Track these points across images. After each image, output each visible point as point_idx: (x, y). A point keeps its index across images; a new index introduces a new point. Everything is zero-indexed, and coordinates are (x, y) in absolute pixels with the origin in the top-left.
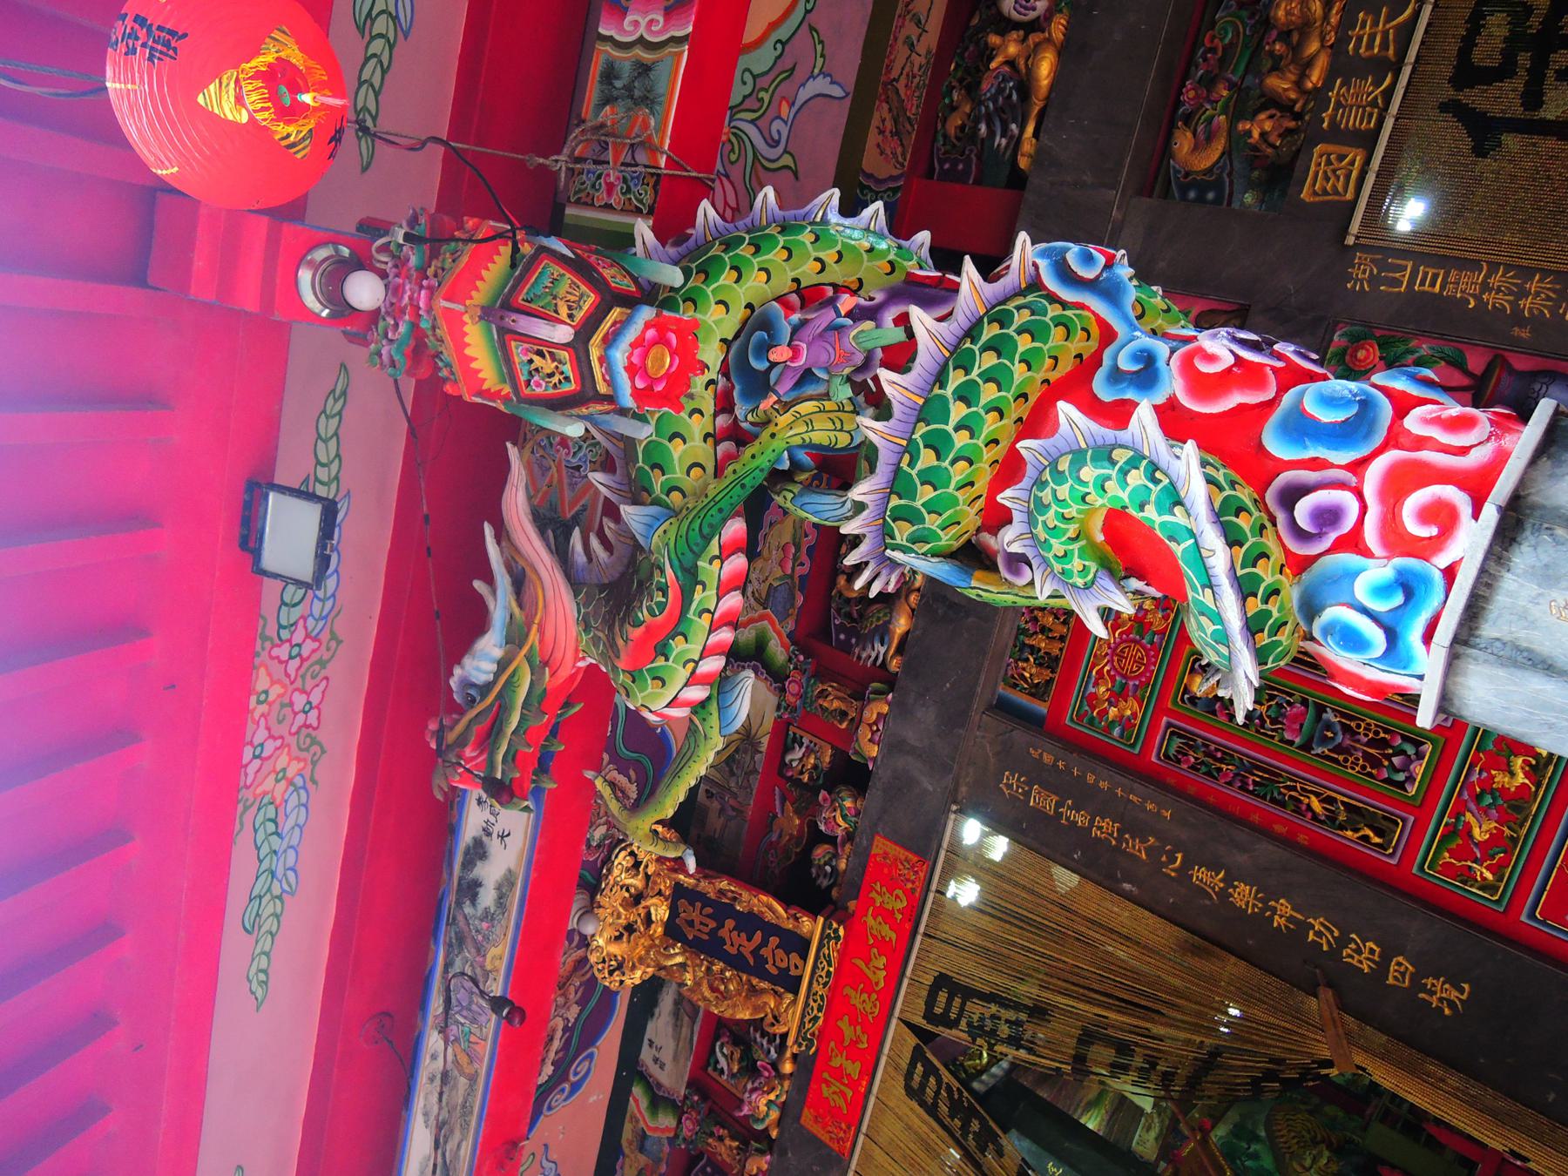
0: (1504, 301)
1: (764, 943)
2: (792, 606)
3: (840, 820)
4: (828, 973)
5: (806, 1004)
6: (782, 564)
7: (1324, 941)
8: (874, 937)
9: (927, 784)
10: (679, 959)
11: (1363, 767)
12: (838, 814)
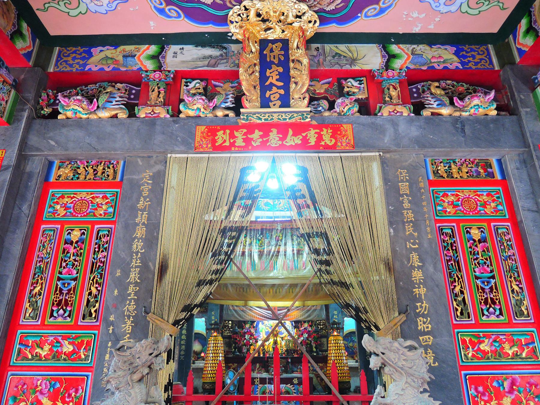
1: (279, 88)
3: (347, 108)
4: (285, 119)
5: (265, 113)
7: (420, 309)
9: (386, 139)
10: (254, 50)
11: (482, 299)
12: (350, 106)
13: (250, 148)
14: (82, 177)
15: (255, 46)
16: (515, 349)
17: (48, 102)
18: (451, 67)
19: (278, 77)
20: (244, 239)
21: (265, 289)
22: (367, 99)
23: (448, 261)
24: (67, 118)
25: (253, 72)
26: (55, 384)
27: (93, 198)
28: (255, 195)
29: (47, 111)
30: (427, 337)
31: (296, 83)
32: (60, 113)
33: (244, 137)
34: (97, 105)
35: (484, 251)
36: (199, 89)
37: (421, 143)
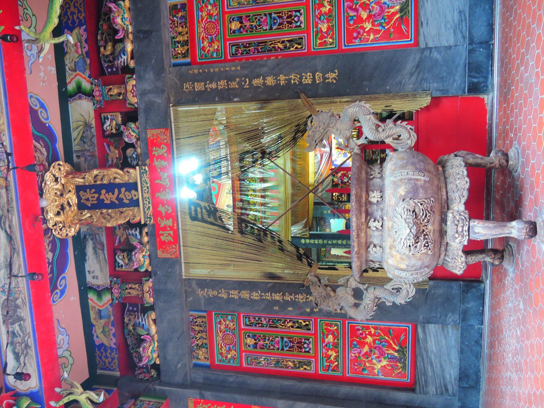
1: (120, 192)
2: (86, 65)
3: (132, 134)
4: (148, 187)
5: (144, 204)
6: (77, 52)
8: (160, 168)
9: (159, 101)
10: (89, 215)
11: (288, 26)
12: (130, 130)
13: (173, 214)
14: (205, 341)
15: (86, 214)
17: (145, 373)
18: (85, 36)
19: (110, 193)
20: (249, 197)
21: (298, 168)
22: (121, 113)
23: (258, 52)
24: (158, 357)
25: (108, 215)
26: (354, 345)
27: (221, 332)
28: (213, 209)
29: (153, 373)
30: (316, 77)
31: (115, 178)
32: (155, 362)
33: (165, 219)
34: (146, 336)
35: (249, 20)
36: (124, 256)
37: (160, 71)
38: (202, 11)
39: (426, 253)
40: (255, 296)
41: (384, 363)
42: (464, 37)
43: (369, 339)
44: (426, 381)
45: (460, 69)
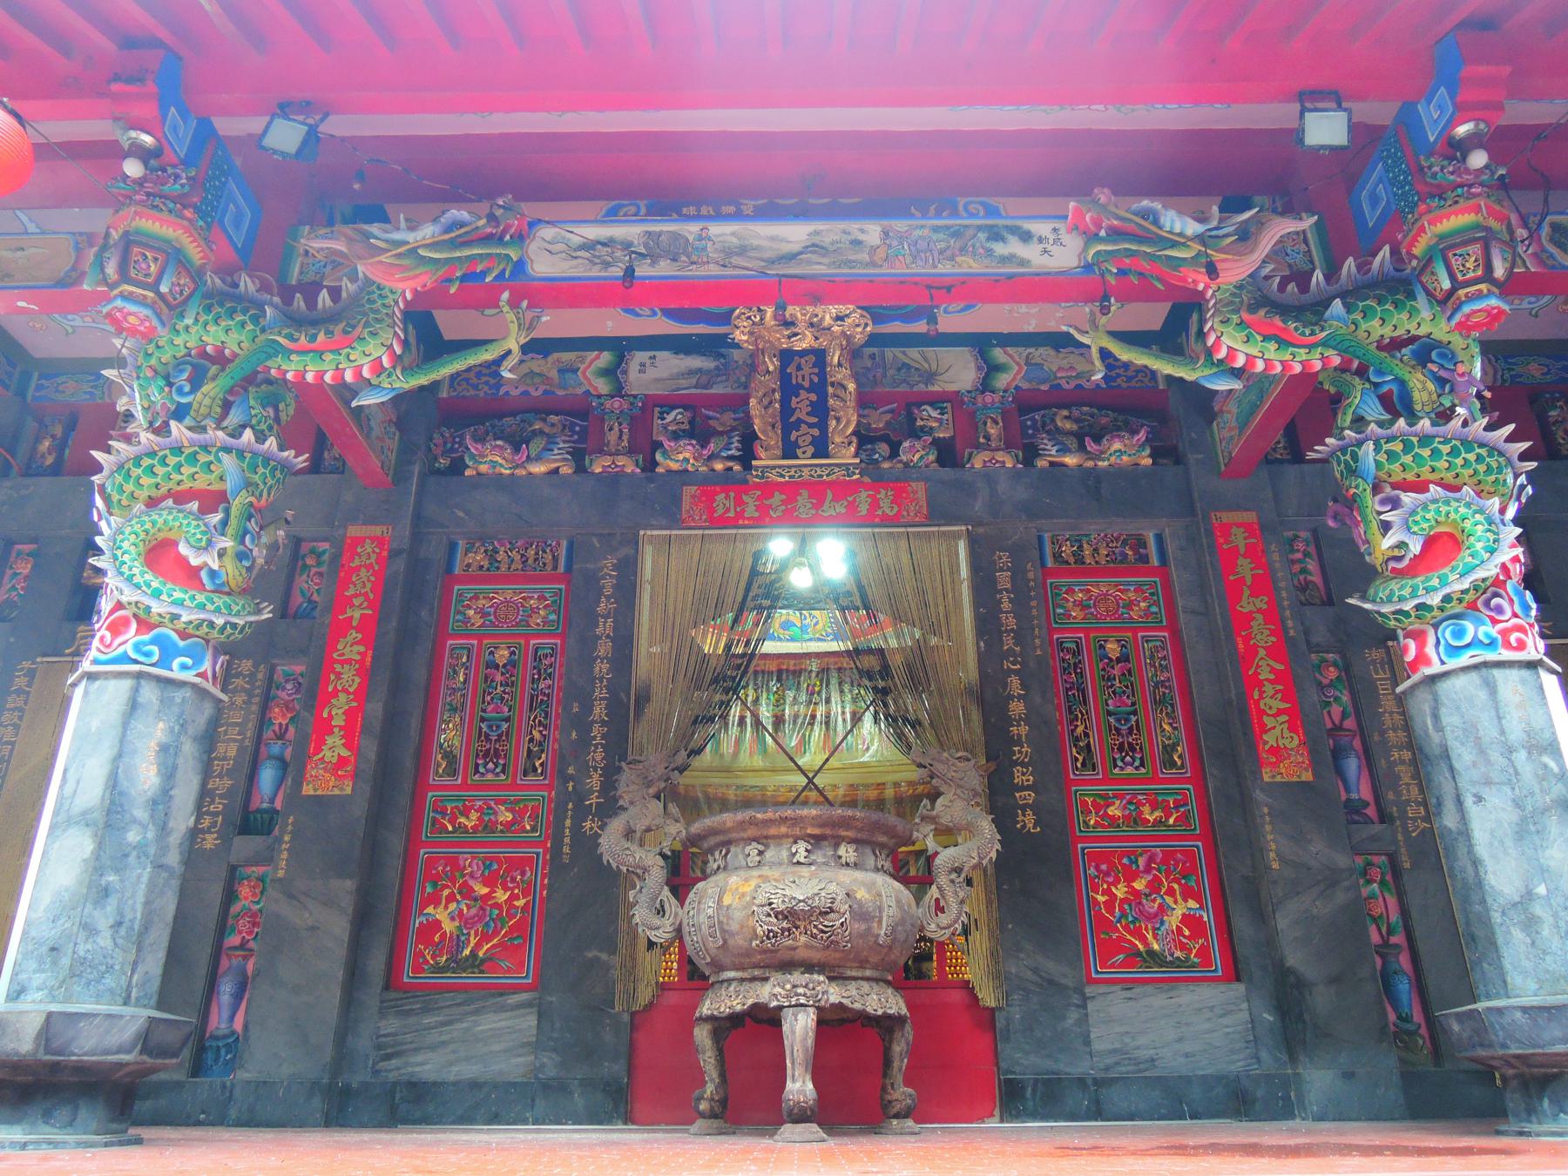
0: (1388, 723)
1: (811, 426)
3: (917, 456)
5: (790, 467)
6: (1060, 369)
9: (978, 506)
10: (771, 368)
14: (504, 568)
16: (1157, 814)
22: (952, 438)
24: (479, 474)
29: (443, 462)
31: (838, 419)
38: (1136, 591)
39: (756, 936)
40: (601, 668)
41: (449, 927)
42: (1107, 1069)
43: (501, 896)
44: (409, 1013)
45: (1048, 1064)
